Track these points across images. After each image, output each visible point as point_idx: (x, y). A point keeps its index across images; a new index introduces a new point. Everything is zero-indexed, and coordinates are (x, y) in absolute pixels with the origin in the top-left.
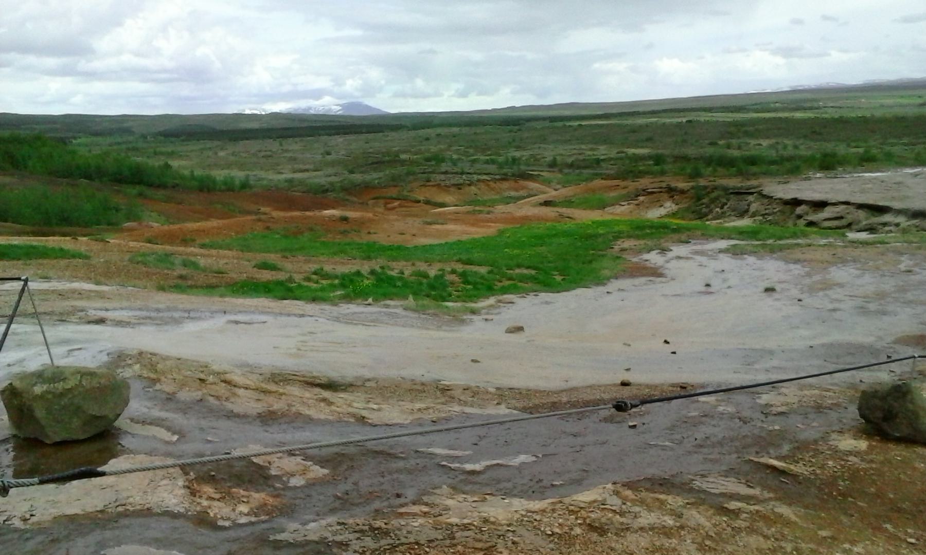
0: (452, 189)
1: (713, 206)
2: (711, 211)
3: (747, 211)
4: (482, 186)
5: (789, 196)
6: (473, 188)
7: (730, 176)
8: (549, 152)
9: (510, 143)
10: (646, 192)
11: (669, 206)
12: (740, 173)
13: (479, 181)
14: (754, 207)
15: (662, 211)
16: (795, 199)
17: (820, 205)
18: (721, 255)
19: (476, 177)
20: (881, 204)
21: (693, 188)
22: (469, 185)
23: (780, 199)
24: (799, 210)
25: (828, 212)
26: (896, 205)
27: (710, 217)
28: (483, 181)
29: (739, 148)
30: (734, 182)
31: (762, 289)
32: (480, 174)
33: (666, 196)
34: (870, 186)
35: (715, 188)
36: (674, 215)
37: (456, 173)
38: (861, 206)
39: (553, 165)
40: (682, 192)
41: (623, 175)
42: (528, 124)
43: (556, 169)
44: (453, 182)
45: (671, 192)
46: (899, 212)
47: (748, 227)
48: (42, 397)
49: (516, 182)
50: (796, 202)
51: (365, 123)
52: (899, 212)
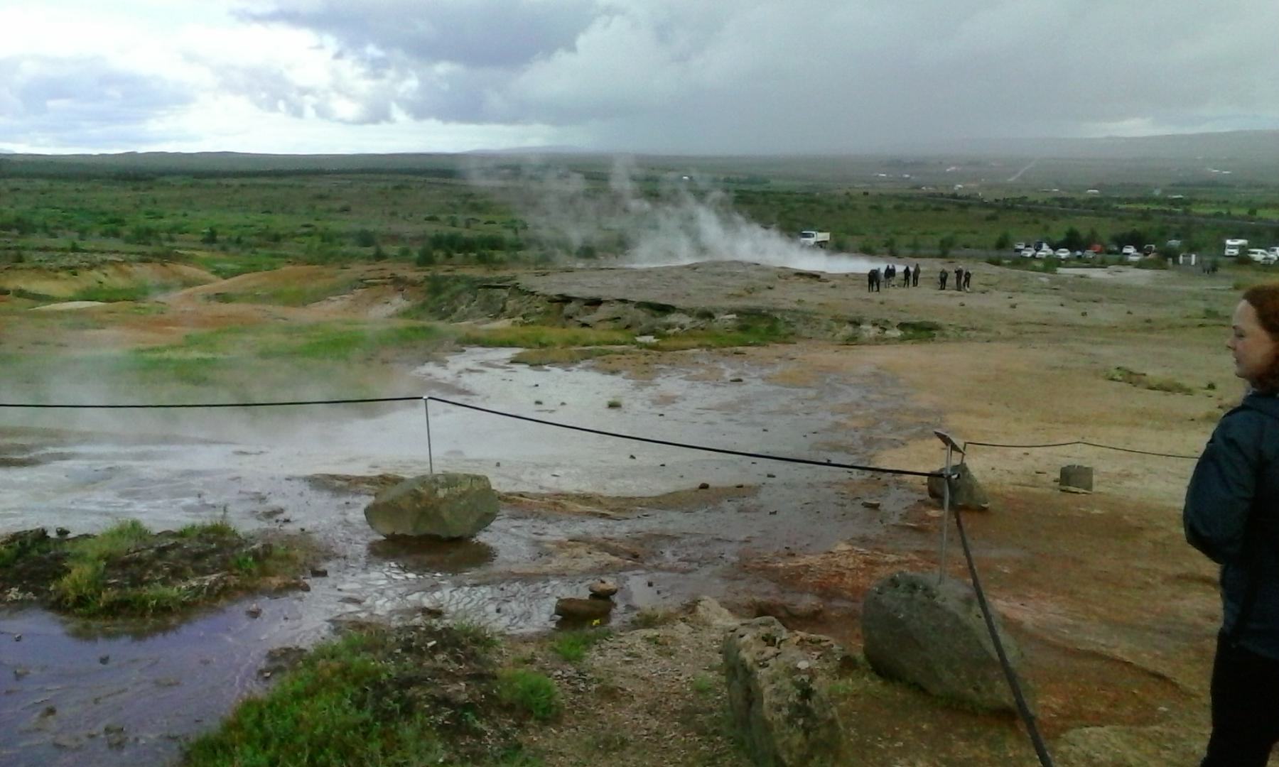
0: (63, 274)
1: (456, 302)
2: (455, 310)
3: (503, 310)
4: (110, 270)
5: (554, 292)
6: (95, 273)
7: (467, 263)
8: (203, 219)
9: (136, 206)
10: (363, 283)
11: (399, 302)
12: (482, 260)
13: (104, 262)
14: (511, 304)
15: (390, 309)
16: (561, 295)
17: (596, 303)
18: (516, 367)
19: (99, 257)
20: (662, 302)
21: (427, 278)
22: (90, 269)
23: (544, 295)
24: (570, 308)
25: (603, 311)
26: (679, 303)
27: (453, 317)
28: (112, 263)
29: (468, 226)
30: (478, 272)
31: (605, 401)
32: (103, 252)
33: (391, 287)
34: (645, 280)
35: (457, 280)
36: (405, 314)
37: (63, 249)
38: (640, 305)
39: (211, 239)
40: (413, 284)
41: (324, 259)
42: (161, 179)
43: (215, 246)
44: (64, 263)
45: (399, 284)
46: (684, 311)
47: (507, 331)
48: (444, 500)
49: (163, 265)
50: (566, 300)
51: (776, 184)
52: (684, 311)
